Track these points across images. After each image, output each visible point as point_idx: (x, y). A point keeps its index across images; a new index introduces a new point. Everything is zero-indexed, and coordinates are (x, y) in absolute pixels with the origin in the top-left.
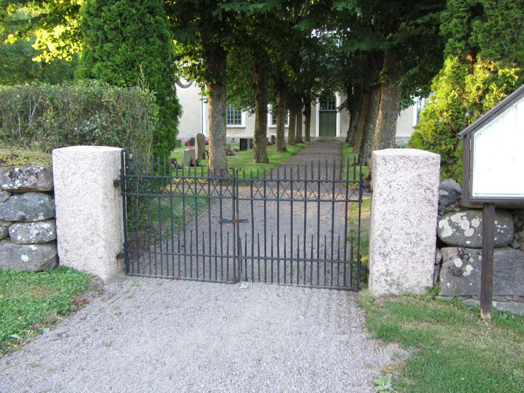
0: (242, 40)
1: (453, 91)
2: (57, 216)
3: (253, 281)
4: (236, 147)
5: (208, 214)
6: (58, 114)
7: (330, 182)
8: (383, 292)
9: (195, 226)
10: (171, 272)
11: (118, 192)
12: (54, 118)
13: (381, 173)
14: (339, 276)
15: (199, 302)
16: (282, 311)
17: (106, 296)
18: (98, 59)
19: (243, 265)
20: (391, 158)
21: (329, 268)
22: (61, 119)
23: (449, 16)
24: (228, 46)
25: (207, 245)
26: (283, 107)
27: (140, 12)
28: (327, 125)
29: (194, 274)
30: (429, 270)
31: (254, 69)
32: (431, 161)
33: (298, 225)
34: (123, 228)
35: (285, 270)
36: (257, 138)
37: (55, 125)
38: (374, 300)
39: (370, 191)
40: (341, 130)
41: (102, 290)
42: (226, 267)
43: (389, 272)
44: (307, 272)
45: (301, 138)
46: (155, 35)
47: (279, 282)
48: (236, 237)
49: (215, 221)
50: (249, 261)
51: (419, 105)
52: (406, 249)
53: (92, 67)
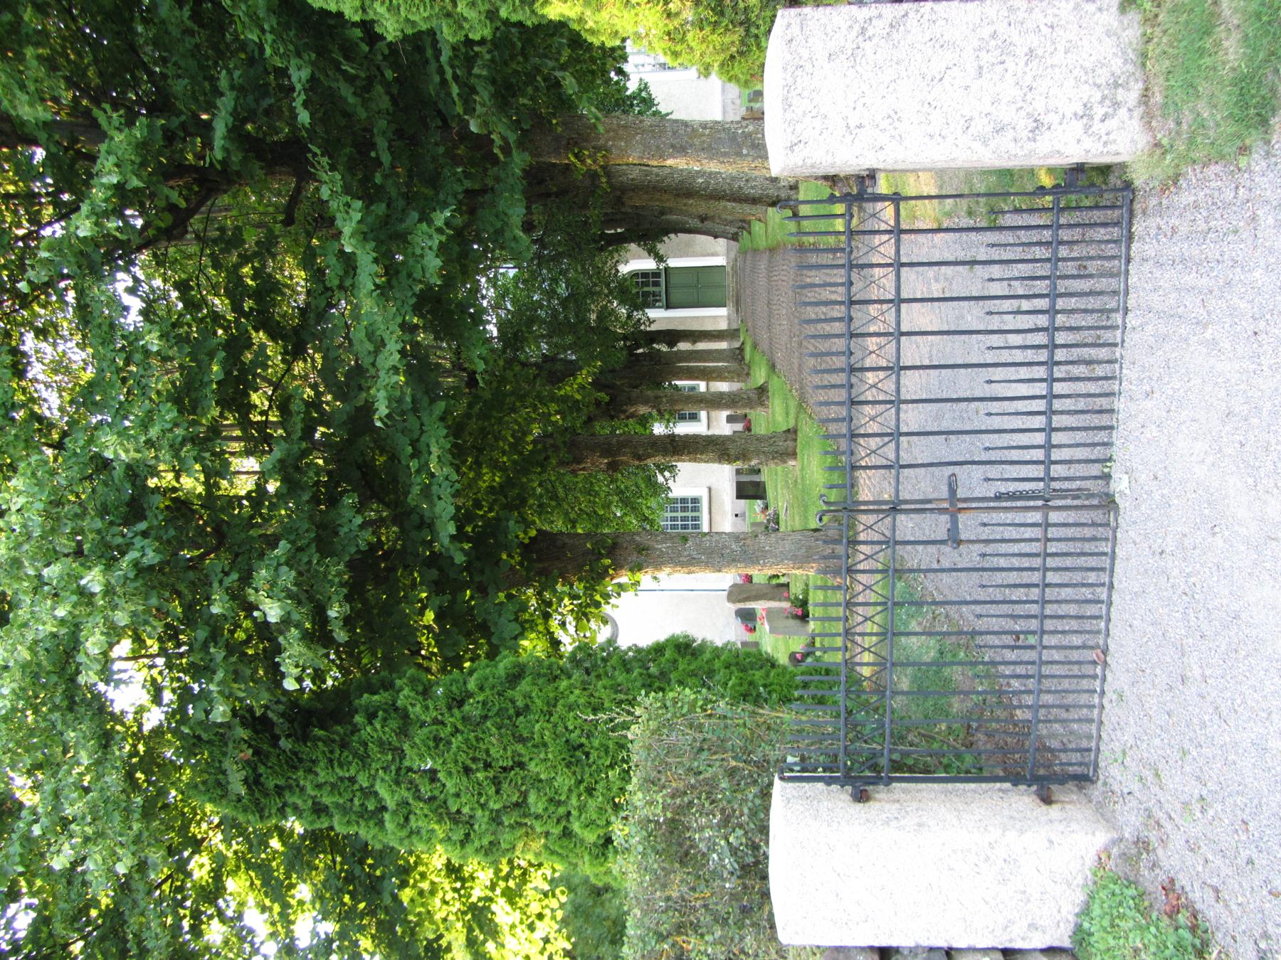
0: (511, 497)
2: (944, 945)
3: (1110, 459)
4: (758, 509)
5: (931, 576)
6: (696, 927)
7: (850, 276)
8: (1135, 125)
9: (964, 608)
10: (1088, 670)
11: (880, 792)
12: (702, 936)
14: (1093, 241)
15: (1170, 599)
16: (1192, 382)
17: (1153, 837)
18: (565, 828)
19: (1066, 485)
21: (1070, 268)
22: (706, 919)
23: (451, 21)
24: (528, 525)
25: (1013, 577)
26: (657, 397)
27: (460, 727)
28: (699, 289)
29: (1091, 610)
30: (1075, 9)
31: (575, 466)
32: (795, 29)
33: (955, 350)
34: (973, 786)
35: (1078, 379)
36: (737, 459)
37: (718, 933)
38: (1157, 145)
39: (872, 175)
41: (1136, 843)
42: (1073, 529)
43: (1081, 113)
44: (1084, 323)
47: (1112, 394)
48: (992, 504)
49: (949, 556)
50: (1057, 471)
51: (640, 70)
52: (1020, 74)
53: (582, 841)
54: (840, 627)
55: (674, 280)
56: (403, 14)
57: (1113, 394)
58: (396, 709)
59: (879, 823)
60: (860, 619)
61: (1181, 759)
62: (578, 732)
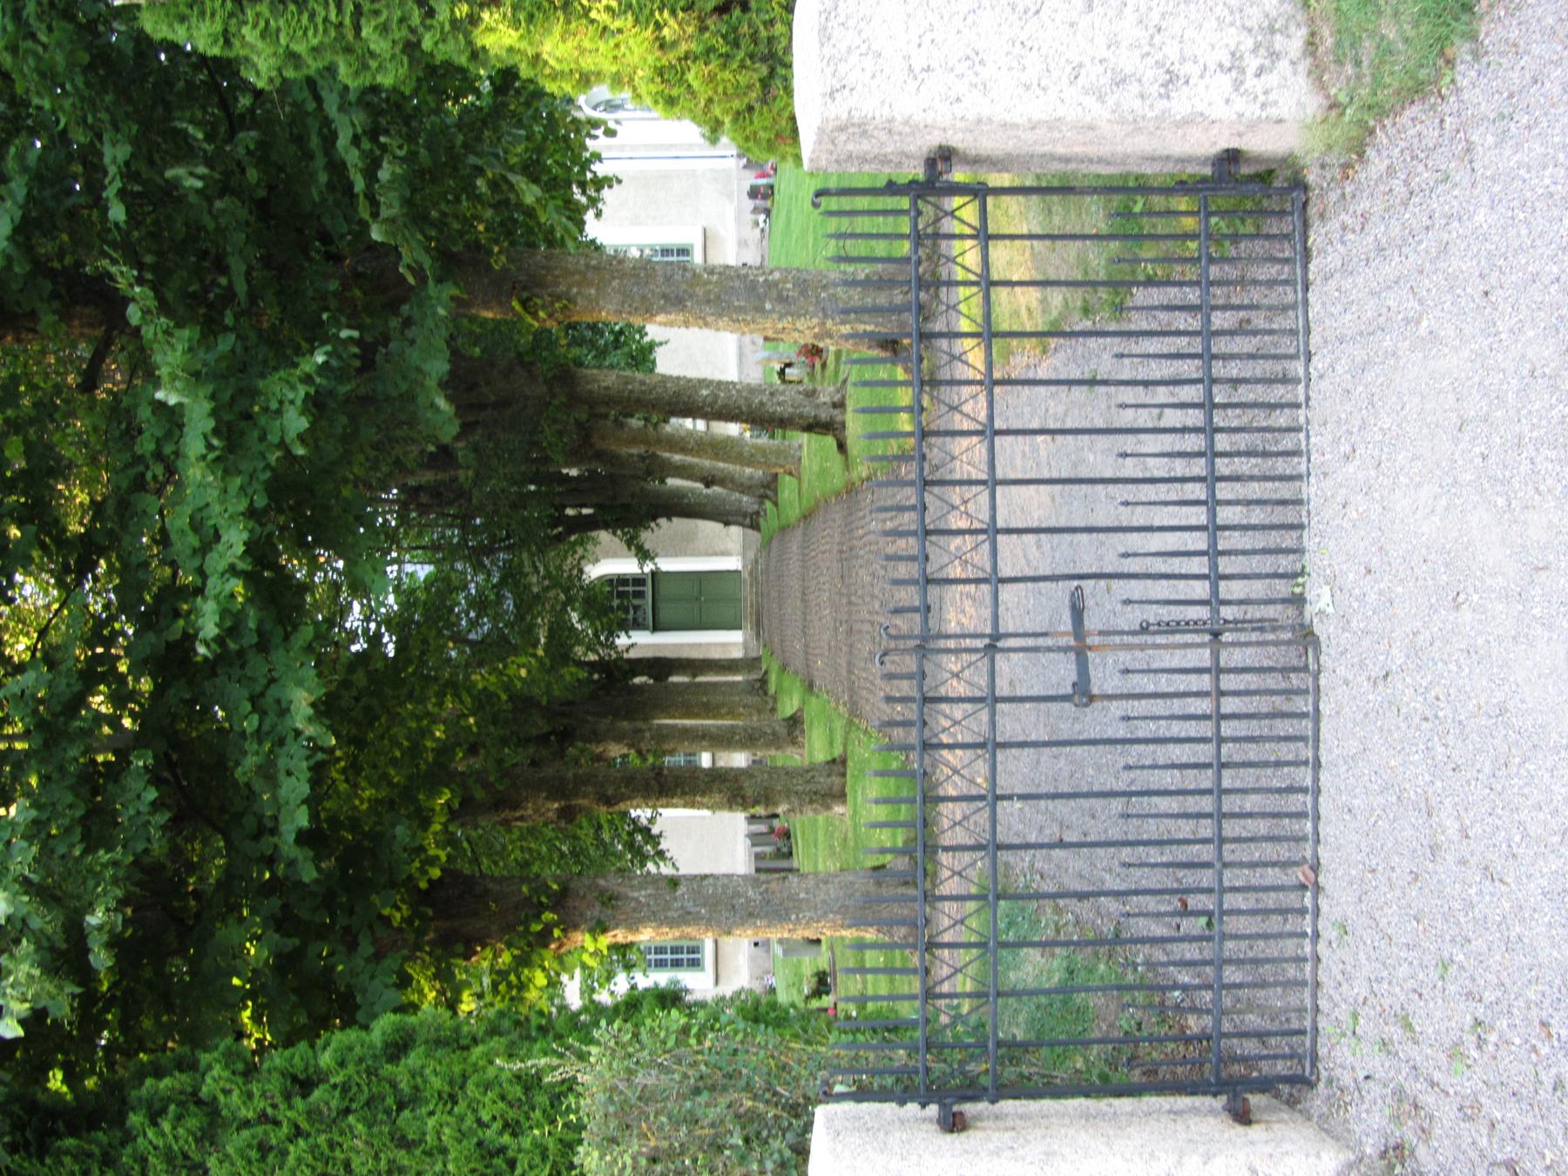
1: (593, 15)
3: (1302, 573)
8: (1301, 83)
13: (883, 102)
20: (829, 71)
23: (352, 59)
27: (304, 1125)
28: (702, 600)
31: (507, 814)
36: (756, 802)
40: (715, 551)
43: (1227, 64)
45: (750, 684)
46: (388, 1068)
52: (1143, 10)
54: (915, 985)
55: (666, 589)
56: (283, 41)
57: (1299, 477)
58: (199, 1102)
59: (983, 1154)
60: (946, 971)
61: (1442, 978)
62: (497, 1125)
